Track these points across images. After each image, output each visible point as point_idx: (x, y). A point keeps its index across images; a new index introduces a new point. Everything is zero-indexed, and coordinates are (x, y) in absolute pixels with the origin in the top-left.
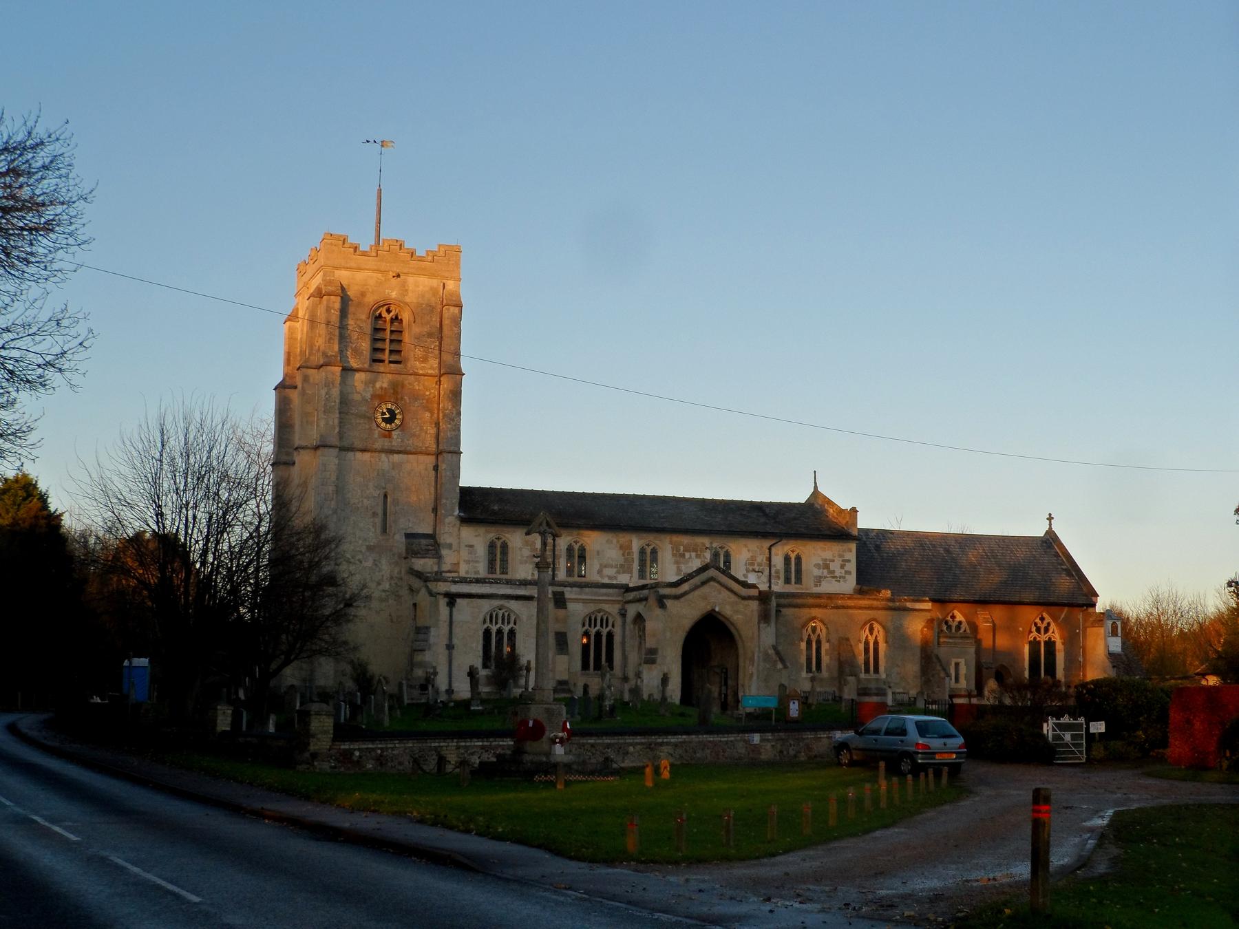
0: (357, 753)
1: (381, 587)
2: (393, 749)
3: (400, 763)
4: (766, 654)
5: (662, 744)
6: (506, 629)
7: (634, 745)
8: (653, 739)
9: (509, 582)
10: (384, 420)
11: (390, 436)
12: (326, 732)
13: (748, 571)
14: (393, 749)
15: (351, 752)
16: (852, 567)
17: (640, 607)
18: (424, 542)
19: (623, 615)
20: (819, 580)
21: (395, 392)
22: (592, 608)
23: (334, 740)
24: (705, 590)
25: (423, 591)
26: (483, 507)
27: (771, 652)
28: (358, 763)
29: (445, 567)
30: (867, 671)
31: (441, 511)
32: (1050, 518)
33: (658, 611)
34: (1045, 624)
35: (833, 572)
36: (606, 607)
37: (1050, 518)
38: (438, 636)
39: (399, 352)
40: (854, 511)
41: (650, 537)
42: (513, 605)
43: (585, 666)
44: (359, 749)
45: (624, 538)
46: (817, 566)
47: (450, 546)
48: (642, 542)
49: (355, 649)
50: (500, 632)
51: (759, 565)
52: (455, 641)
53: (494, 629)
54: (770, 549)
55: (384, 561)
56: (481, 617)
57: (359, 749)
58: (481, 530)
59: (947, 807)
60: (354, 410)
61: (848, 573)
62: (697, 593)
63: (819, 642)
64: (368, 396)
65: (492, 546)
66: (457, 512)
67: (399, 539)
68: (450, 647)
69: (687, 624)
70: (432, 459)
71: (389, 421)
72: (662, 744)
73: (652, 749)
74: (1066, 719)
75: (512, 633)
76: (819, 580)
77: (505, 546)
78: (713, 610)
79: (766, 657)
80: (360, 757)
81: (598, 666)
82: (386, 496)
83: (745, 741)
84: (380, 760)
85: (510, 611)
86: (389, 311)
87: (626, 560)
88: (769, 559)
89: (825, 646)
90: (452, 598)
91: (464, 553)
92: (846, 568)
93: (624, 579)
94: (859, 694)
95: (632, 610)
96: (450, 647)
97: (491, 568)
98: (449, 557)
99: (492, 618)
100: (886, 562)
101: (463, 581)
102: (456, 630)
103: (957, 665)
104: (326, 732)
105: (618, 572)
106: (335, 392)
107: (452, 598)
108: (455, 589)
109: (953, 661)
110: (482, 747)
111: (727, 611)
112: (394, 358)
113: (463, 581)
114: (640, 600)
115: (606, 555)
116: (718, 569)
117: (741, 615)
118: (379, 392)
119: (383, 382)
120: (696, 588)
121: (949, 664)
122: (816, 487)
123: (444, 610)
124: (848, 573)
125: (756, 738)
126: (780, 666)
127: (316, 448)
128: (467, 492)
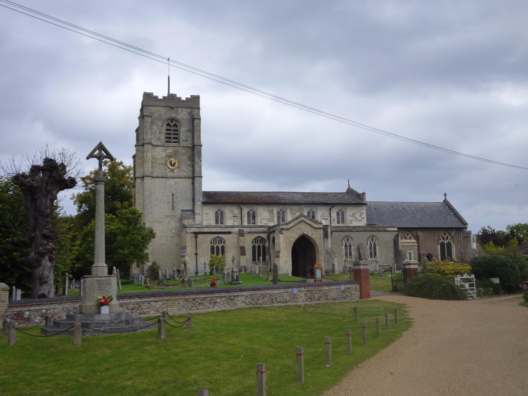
0: (27, 313)
1: (172, 232)
2: (54, 309)
5: (237, 296)
7: (220, 297)
8: (232, 294)
11: (173, 171)
13: (321, 219)
14: (54, 309)
16: (364, 216)
20: (351, 221)
22: (256, 235)
24: (300, 225)
26: (214, 199)
28: (28, 319)
29: (197, 223)
30: (371, 256)
32: (445, 195)
34: (446, 236)
35: (357, 218)
37: (445, 195)
40: (364, 194)
41: (281, 207)
42: (221, 235)
43: (254, 259)
44: (29, 311)
45: (270, 208)
46: (350, 216)
50: (217, 247)
51: (326, 216)
52: (198, 252)
53: (257, 245)
54: (330, 210)
59: (367, 360)
61: (363, 218)
62: (296, 227)
64: (164, 156)
65: (216, 213)
69: (293, 240)
72: (237, 296)
73: (232, 300)
74: (465, 276)
75: (223, 247)
76: (351, 221)
77: (222, 213)
80: (30, 315)
86: (172, 122)
87: (271, 217)
88: (330, 214)
89: (353, 247)
92: (362, 216)
94: (354, 265)
100: (381, 217)
103: (410, 253)
105: (268, 222)
109: (408, 252)
111: (310, 234)
115: (265, 217)
116: (305, 217)
117: (316, 236)
119: (170, 151)
120: (296, 225)
121: (406, 253)
122: (349, 186)
124: (363, 218)
125: (295, 291)
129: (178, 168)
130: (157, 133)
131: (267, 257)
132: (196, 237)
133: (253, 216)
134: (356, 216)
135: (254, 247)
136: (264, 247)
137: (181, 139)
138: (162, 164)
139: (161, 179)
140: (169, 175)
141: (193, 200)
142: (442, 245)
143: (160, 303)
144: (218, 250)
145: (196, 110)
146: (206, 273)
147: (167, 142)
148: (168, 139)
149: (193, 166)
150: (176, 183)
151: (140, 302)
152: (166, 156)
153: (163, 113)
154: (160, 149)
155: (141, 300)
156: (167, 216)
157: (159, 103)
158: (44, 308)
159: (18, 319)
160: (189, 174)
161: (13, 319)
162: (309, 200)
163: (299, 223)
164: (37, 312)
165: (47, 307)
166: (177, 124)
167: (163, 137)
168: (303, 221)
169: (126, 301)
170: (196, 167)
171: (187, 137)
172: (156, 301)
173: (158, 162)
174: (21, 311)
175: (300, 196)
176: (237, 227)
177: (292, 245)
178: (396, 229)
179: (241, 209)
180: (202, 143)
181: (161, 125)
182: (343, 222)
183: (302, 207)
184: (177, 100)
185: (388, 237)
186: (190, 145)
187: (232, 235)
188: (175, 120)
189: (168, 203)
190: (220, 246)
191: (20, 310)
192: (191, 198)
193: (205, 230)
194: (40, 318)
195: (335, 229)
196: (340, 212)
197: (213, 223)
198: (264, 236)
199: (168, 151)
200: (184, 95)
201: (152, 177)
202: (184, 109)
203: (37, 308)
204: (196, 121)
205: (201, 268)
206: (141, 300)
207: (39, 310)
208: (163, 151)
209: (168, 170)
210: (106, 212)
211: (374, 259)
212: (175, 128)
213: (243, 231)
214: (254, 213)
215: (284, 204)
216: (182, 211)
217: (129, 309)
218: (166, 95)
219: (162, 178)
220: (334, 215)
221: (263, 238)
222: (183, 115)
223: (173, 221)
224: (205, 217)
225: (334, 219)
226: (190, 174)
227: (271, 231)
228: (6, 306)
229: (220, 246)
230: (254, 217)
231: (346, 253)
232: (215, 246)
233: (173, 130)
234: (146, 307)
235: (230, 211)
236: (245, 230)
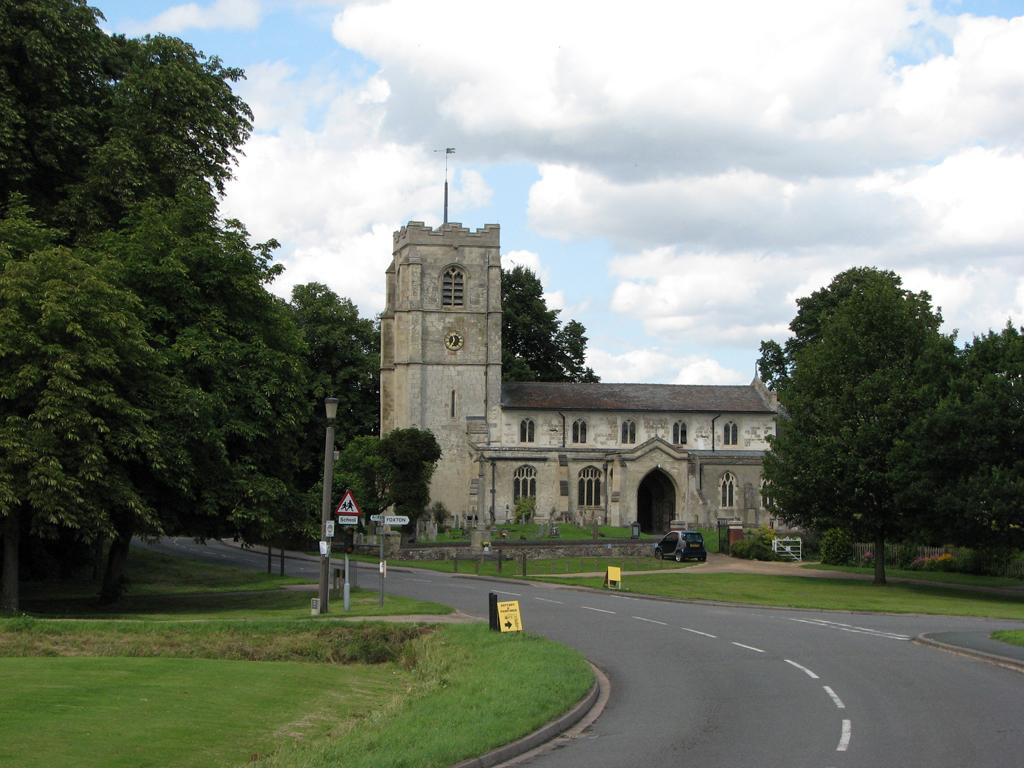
4: (693, 496)
11: (455, 354)
13: (698, 436)
19: (606, 470)
27: (696, 493)
30: (724, 504)
31: (490, 403)
35: (759, 436)
36: (595, 464)
39: (462, 284)
41: (630, 416)
42: (531, 463)
43: (581, 502)
45: (611, 417)
46: (748, 432)
47: (495, 425)
48: (625, 420)
49: (429, 483)
50: (525, 481)
53: (586, 479)
56: (513, 471)
58: (515, 414)
60: (431, 338)
63: (731, 486)
64: (440, 328)
67: (463, 421)
69: (641, 476)
75: (533, 481)
76: (748, 442)
81: (589, 503)
82: (453, 393)
89: (735, 489)
106: (419, 328)
108: (494, 455)
112: (458, 294)
117: (677, 471)
118: (449, 325)
131: (602, 498)
132: (494, 465)
134: (758, 432)
135: (581, 482)
136: (598, 482)
137: (468, 299)
140: (447, 361)
144: (524, 489)
146: (508, 521)
148: (446, 300)
150: (459, 373)
152: (444, 328)
153: (440, 256)
157: (434, 240)
160: (480, 357)
162: (678, 403)
163: (651, 451)
167: (438, 296)
176: (557, 450)
179: (564, 419)
181: (436, 276)
182: (735, 442)
186: (483, 311)
187: (547, 464)
189: (446, 405)
190: (529, 479)
192: (484, 398)
193: (508, 455)
195: (708, 461)
196: (731, 426)
197: (517, 437)
198: (599, 465)
199: (447, 320)
200: (473, 225)
205: (500, 510)
208: (439, 321)
210: (704, 560)
211: (730, 508)
212: (458, 280)
213: (565, 456)
215: (633, 411)
216: (468, 418)
219: (438, 364)
220: (720, 431)
221: (597, 470)
222: (472, 257)
225: (719, 437)
227: (608, 457)
229: (529, 479)
231: (724, 498)
232: (521, 479)
236: (569, 455)
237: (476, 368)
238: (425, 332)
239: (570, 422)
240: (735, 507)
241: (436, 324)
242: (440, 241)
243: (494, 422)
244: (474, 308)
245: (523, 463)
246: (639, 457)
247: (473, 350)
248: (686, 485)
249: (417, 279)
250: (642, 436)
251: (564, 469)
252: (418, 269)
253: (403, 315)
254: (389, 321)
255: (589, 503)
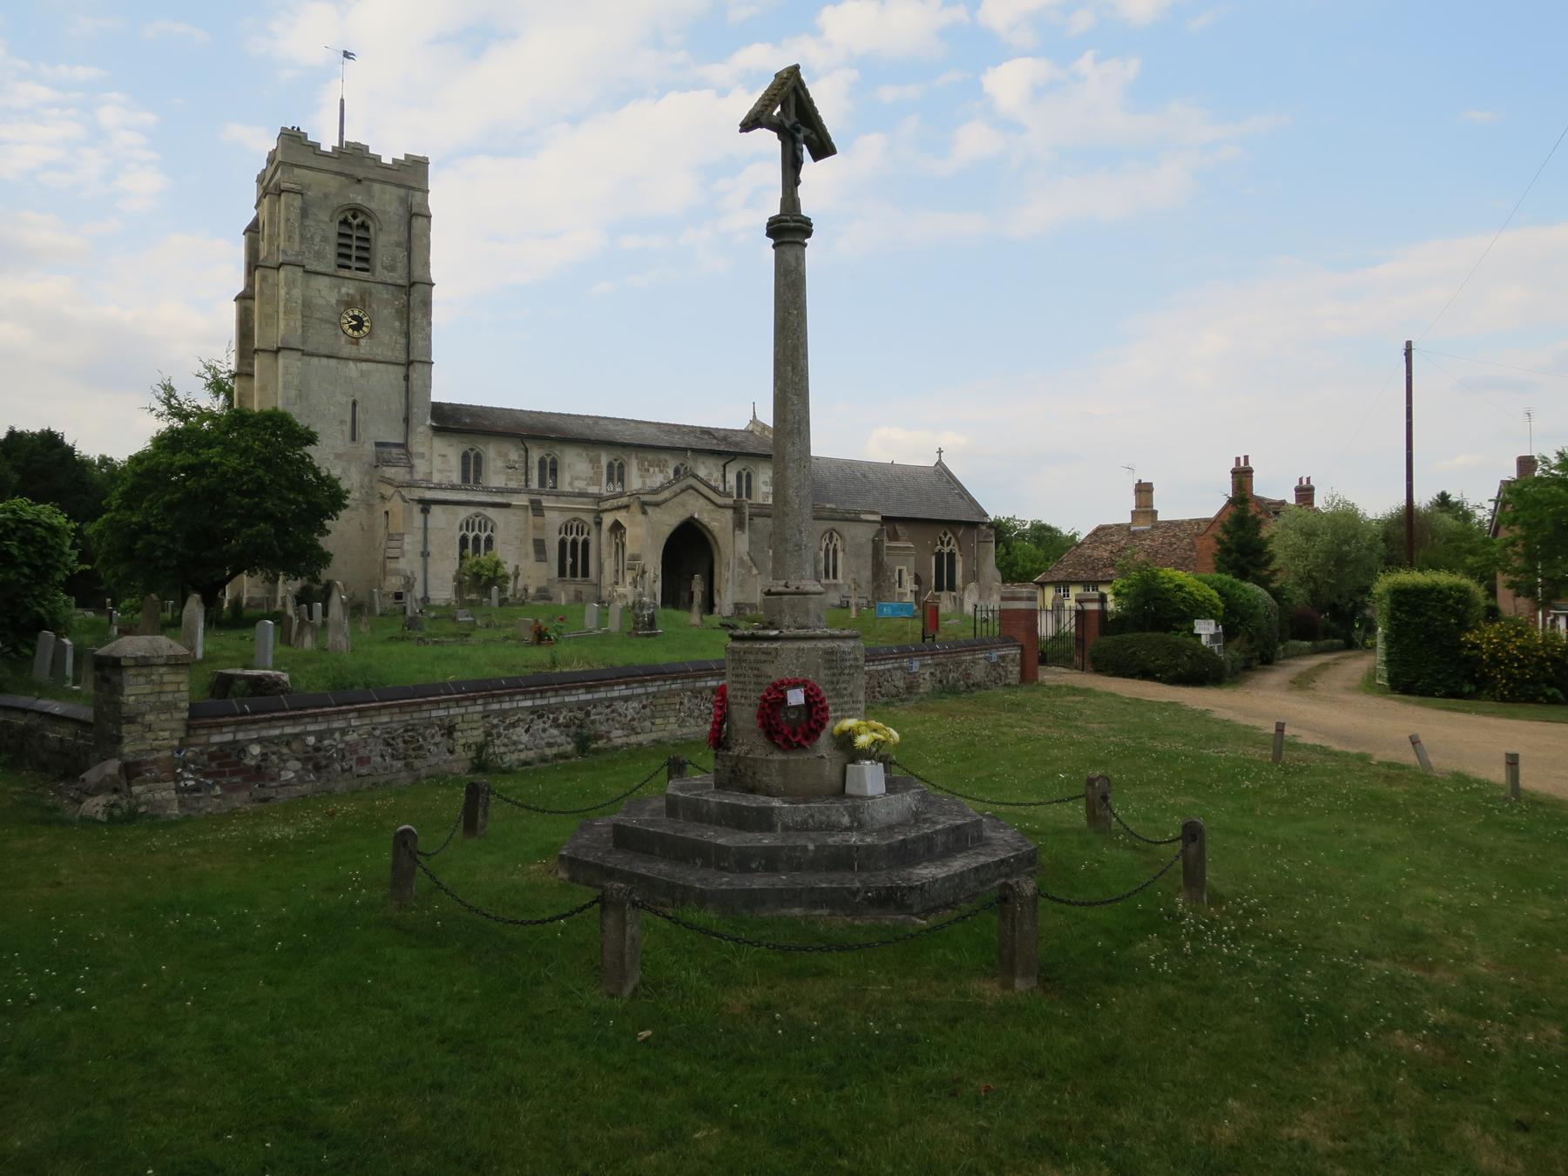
0: (256, 750)
2: (343, 732)
3: (362, 761)
4: (742, 562)
6: (483, 536)
9: (487, 490)
10: (352, 327)
12: (171, 707)
14: (343, 732)
15: (240, 749)
17: (621, 516)
18: (395, 451)
19: (599, 524)
21: (363, 300)
23: (190, 728)
25: (397, 498)
26: (450, 421)
27: (746, 558)
28: (259, 773)
31: (414, 421)
32: (940, 452)
33: (640, 517)
38: (411, 543)
41: (618, 453)
42: (490, 513)
43: (562, 573)
44: (259, 741)
47: (422, 456)
48: (612, 458)
50: (574, 542)
52: (431, 548)
53: (471, 535)
55: (353, 470)
57: (259, 741)
63: (835, 551)
64: (333, 301)
65: (465, 457)
66: (429, 422)
67: (369, 448)
68: (425, 554)
70: (401, 371)
71: (358, 328)
77: (478, 457)
78: (692, 518)
79: (742, 563)
80: (264, 756)
81: (574, 574)
82: (354, 404)
83: (902, 668)
84: (315, 761)
85: (487, 519)
90: (426, 505)
91: (437, 462)
93: (593, 490)
95: (608, 520)
96: (425, 554)
97: (465, 478)
98: (421, 467)
99: (468, 525)
101: (439, 487)
102: (431, 537)
104: (171, 707)
107: (426, 505)
108: (429, 495)
110: (532, 710)
113: (439, 487)
114: (618, 508)
117: (718, 522)
119: (349, 289)
123: (418, 518)
126: (755, 571)
127: (279, 350)
128: (439, 411)
129: (370, 334)
130: (317, 239)
133: (550, 469)
135: (562, 543)
138: (327, 321)
139: (324, 361)
141: (407, 420)
142: (939, 556)
143: (635, 704)
145: (419, 195)
147: (341, 266)
149: (407, 335)
150: (363, 374)
151: (588, 702)
152: (339, 302)
154: (322, 283)
155: (589, 697)
156: (338, 456)
158: (311, 728)
159: (222, 774)
161: (207, 776)
163: (683, 491)
164: (288, 744)
165: (323, 727)
166: (370, 223)
167: (331, 252)
168: (692, 487)
169: (552, 701)
170: (416, 336)
171: (394, 259)
172: (626, 699)
173: (318, 315)
174: (235, 742)
175: (653, 430)
177: (662, 542)
178: (878, 518)
180: (434, 277)
183: (663, 456)
184: (371, 163)
185: (862, 535)
186: (400, 282)
188: (363, 212)
191: (228, 737)
192: (402, 415)
194: (298, 765)
197: (456, 478)
200: (389, 150)
201: (304, 353)
202: (388, 188)
203: (288, 730)
204: (418, 223)
206: (589, 697)
207: (296, 736)
209: (343, 338)
211: (831, 581)
212: (361, 233)
214: (554, 462)
216: (378, 444)
217: (558, 726)
218: (337, 144)
222: (383, 201)
223: (353, 470)
224: (437, 462)
226: (402, 358)
228: (181, 726)
230: (554, 472)
233: (358, 238)
234: (603, 718)
235: (500, 454)
237: (391, 367)
238: (307, 305)
239: (535, 455)
240: (840, 580)
241: (326, 292)
242: (334, 166)
243: (421, 450)
244: (389, 277)
245: (472, 510)
246: (666, 501)
247: (386, 339)
248: (733, 547)
249: (295, 214)
250: (635, 481)
251: (539, 519)
252: (297, 202)
253: (269, 272)
254: (249, 302)
255: (574, 574)
